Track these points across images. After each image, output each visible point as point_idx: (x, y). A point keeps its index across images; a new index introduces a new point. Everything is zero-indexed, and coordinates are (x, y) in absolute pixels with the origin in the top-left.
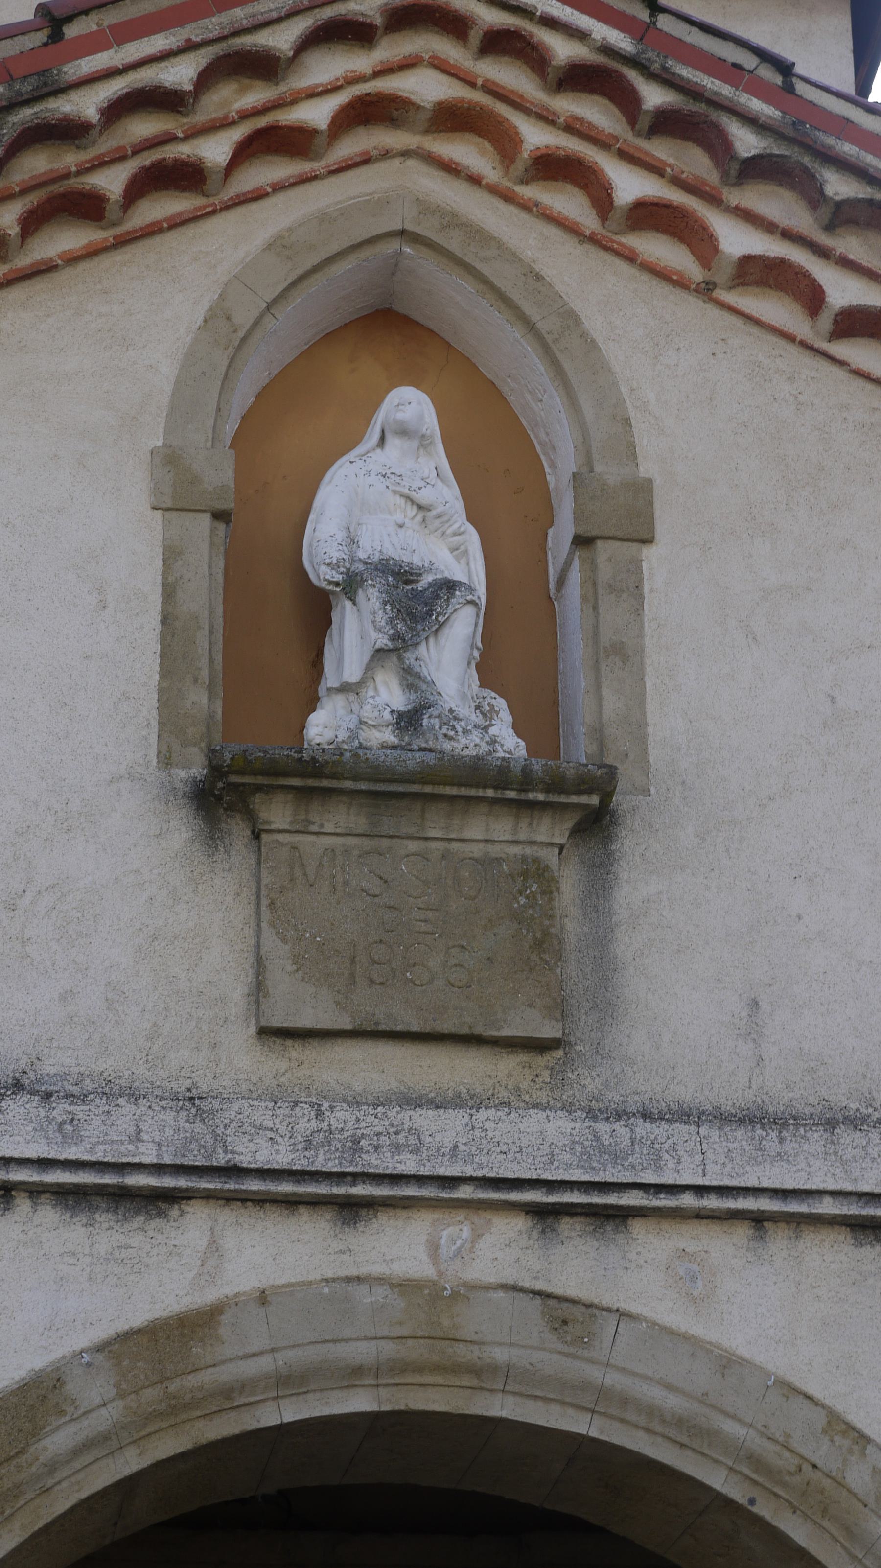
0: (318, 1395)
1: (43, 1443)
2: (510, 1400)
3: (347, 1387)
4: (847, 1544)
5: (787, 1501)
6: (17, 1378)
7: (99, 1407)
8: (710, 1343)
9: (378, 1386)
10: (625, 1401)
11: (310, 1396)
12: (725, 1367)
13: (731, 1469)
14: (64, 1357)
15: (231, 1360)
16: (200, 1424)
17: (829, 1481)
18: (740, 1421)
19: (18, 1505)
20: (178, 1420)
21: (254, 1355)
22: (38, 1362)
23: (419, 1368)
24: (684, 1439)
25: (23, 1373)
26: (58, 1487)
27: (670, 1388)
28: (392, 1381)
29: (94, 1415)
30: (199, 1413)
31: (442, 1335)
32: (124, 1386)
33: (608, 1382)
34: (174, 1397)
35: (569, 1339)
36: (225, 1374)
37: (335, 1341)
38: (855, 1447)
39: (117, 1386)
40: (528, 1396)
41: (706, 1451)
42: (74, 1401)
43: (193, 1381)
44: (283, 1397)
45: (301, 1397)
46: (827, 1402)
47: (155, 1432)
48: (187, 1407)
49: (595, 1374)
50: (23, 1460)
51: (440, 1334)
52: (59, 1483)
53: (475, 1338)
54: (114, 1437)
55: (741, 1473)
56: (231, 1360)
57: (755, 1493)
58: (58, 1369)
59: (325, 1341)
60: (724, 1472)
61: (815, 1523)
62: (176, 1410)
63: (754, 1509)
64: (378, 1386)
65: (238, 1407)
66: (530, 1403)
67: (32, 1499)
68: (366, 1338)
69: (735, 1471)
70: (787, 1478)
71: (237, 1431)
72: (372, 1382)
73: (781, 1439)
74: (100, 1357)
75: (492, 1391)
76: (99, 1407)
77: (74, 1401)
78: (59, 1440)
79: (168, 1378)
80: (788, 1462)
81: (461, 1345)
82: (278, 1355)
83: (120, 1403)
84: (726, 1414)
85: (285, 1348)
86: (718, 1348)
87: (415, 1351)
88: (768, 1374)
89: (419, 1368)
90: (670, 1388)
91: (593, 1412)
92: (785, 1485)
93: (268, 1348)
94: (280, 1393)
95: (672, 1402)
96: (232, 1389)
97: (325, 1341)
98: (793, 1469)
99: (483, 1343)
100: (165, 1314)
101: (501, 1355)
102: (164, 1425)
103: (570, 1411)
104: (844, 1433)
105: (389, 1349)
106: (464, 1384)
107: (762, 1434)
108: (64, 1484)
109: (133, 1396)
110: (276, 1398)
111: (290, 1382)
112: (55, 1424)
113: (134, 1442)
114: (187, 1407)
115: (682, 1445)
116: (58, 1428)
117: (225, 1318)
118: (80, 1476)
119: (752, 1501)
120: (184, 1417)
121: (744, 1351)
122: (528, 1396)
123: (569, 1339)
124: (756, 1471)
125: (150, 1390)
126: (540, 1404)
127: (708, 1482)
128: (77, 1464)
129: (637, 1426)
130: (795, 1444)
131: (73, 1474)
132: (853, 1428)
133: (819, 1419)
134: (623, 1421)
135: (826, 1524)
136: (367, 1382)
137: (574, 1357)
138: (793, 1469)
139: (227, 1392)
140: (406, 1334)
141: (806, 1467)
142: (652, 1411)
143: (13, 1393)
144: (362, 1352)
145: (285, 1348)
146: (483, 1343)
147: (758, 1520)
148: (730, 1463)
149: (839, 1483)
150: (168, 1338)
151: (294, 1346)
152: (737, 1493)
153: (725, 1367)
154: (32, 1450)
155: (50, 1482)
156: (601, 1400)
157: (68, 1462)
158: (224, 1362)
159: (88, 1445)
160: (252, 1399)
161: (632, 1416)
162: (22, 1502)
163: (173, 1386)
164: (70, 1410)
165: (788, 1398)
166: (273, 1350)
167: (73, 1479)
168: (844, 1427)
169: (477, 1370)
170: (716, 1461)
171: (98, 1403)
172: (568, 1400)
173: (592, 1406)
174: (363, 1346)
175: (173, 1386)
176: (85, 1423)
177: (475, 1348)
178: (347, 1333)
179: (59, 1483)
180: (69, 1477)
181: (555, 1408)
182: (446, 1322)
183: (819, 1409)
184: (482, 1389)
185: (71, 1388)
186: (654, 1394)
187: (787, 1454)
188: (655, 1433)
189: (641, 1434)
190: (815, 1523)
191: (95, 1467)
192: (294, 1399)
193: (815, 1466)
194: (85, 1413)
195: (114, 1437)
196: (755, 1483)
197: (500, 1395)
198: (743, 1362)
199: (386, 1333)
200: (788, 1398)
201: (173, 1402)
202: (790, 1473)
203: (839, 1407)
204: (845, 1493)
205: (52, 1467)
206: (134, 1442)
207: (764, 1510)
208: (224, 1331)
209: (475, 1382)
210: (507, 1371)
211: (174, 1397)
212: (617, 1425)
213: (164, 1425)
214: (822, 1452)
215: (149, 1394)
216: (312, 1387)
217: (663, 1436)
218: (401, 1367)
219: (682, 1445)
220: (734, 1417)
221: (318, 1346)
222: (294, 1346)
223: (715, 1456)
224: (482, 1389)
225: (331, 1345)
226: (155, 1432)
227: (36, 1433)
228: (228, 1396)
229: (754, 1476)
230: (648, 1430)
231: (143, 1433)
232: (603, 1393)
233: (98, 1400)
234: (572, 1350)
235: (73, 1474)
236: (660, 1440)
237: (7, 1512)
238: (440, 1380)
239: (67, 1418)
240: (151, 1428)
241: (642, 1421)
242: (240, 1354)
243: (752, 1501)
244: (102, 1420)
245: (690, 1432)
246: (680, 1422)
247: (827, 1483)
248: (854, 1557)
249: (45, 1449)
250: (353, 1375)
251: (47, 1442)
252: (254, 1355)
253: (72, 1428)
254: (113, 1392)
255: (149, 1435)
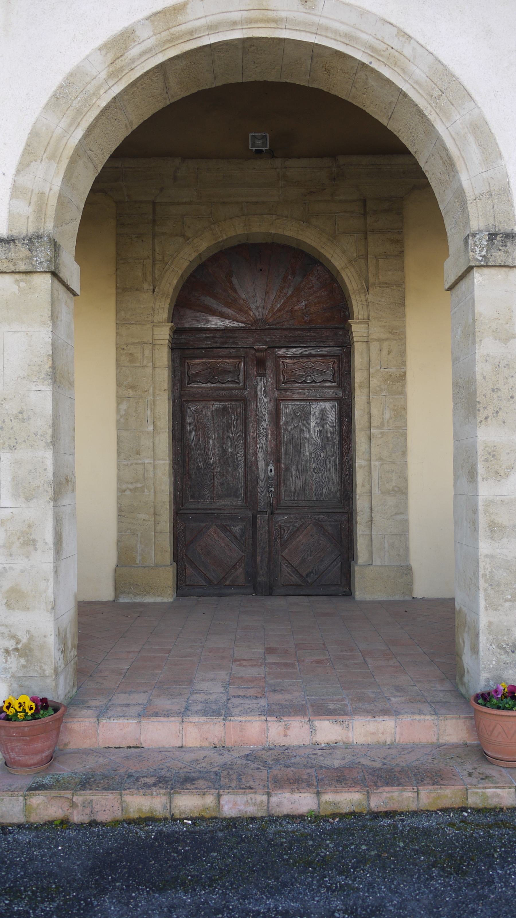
0: (223, 33)
1: (129, 52)
2: (288, 31)
3: (232, 30)
4: (403, 76)
5: (383, 62)
6: (119, 30)
7: (147, 39)
8: (356, 6)
9: (242, 29)
10: (327, 29)
11: (219, 34)
12: (362, 15)
13: (364, 52)
14: (135, 22)
15: (191, 21)
16: (183, 45)
17: (397, 53)
18: (367, 33)
19: (123, 75)
20: (175, 44)
21: (199, 18)
22: (126, 24)
23: (256, 21)
24: (347, 42)
25: (121, 28)
26: (136, 68)
27: (342, 23)
28: (247, 27)
29: (145, 42)
30: (182, 41)
31: (263, 8)
32: (155, 31)
33: (321, 22)
34: (173, 35)
35: (307, 7)
36: (189, 26)
37: (226, 12)
38: (407, 41)
39: (153, 31)
40: (294, 30)
41: (355, 46)
42: (139, 37)
43: (178, 28)
44: (210, 34)
45: (217, 34)
46: (398, 25)
47: (168, 48)
48: (178, 38)
49: (316, 19)
50: (122, 58)
51: (262, 8)
52: (136, 66)
53: (274, 9)
54: (153, 50)
55: (367, 53)
56: (191, 21)
57: (372, 60)
58: (133, 27)
59: (223, 13)
60: (361, 53)
61: (393, 69)
62: (173, 40)
63: (371, 65)
64: (242, 29)
65: (195, 38)
66: (295, 32)
67: (128, 73)
68: (237, 11)
69: (365, 53)
70: (383, 53)
71: (195, 47)
72: (241, 27)
73: (381, 39)
74: (147, 22)
75: (281, 29)
76: (147, 39)
77: (139, 37)
78: (134, 51)
79: (170, 28)
80: (383, 47)
81: (270, 11)
82: (207, 18)
83: (154, 37)
84: (361, 31)
85: (209, 15)
86: (360, 8)
87: (254, 14)
88: (376, 15)
89: (256, 21)
90: (342, 23)
91: (316, 34)
92: (382, 56)
93: (204, 16)
94: (209, 33)
95: (343, 28)
96: (192, 32)
97: (223, 13)
98: (384, 49)
99: (277, 10)
100: (168, 6)
101: (283, 14)
102: (493, 785)
103: (308, 34)
104: (403, 36)
105: (245, 14)
106: (272, 26)
107: (374, 37)
108: (138, 67)
109: (159, 35)
110: (208, 35)
111: (212, 28)
112: (133, 45)
113: (161, 52)
114: (178, 38)
115: (347, 44)
116: (134, 47)
117: (189, 6)
118: (143, 64)
119: (371, 63)
120: (177, 42)
121: (368, 8)
122: (294, 30)
123: (307, 7)
124: (372, 52)
125: (164, 33)
126: (298, 32)
127: (356, 57)
128: (142, 60)
129: (331, 39)
130: (385, 41)
131: (141, 63)
132: (406, 34)
133: (394, 31)
134: (326, 37)
135: (396, 69)
136: (239, 28)
137: (310, 14)
138: (384, 49)
139: (191, 32)
140: (251, 8)
141: (390, 49)
142: (336, 32)
143: (119, 36)
144: (236, 16)
145: (209, 15)
146: (277, 10)
147: (373, 70)
148: (363, 50)
149: (401, 54)
150: (170, 14)
151: (212, 15)
152: (365, 60)
153: (362, 15)
154: (126, 55)
155: (133, 67)
156: (319, 29)
157: (138, 59)
158: (189, 21)
159: (144, 53)
160: (200, 35)
161: (329, 35)
162: (124, 73)
163: (172, 31)
164: (137, 40)
165: (384, 24)
166: (205, 16)
167: (141, 65)
168: (403, 34)
169: (275, 21)
170: (358, 49)
171: (147, 38)
172: (308, 30)
173: (315, 32)
174: (236, 13)
175: (172, 31)
176: (143, 44)
177: (275, 12)
178: (231, 9)
179: (136, 66)
180: (139, 65)
181: (303, 34)
182: (264, 3)
183: (395, 28)
184: (278, 28)
185: (137, 33)
186: (336, 25)
187: (383, 44)
188: (337, 41)
189: (333, 41)
190: (393, 69)
191: (148, 61)
192: (214, 35)
193: (392, 48)
194: (143, 41)
195: (153, 50)
196: (372, 56)
197: (284, 30)
198: (369, 12)
199: (244, 9)
200: (384, 24)
201: (172, 36)
202: (384, 51)
203: (401, 26)
204: (403, 57)
205: (133, 60)
206: (161, 52)
207: (375, 65)
208: (188, 11)
209: (275, 26)
210: (286, 20)
211: (173, 35)
212: (324, 38)
213: (170, 45)
214: (395, 43)
215: (164, 34)
216: (220, 30)
217: (340, 42)
218: (250, 21)
219: (347, 44)
220: (364, 32)
221: (221, 14)
222: (212, 15)
223: (358, 47)
224: (278, 28)
225: (225, 14)
226: (168, 48)
227: (127, 49)
228: (191, 34)
229: (371, 54)
230: (335, 40)
231: (164, 48)
232: (319, 26)
233: (147, 37)
234: (308, 11)
235: (141, 63)
236: (339, 43)
237: (120, 77)
238: (263, 25)
239: (137, 43)
240: (166, 47)
241: (333, 36)
242: (194, 18)
243: (371, 63)
244: (148, 44)
245: (350, 39)
246: (346, 35)
247: (397, 53)
248: (405, 80)
249: (130, 54)
250: (234, 24)
251: (130, 52)
252: (199, 18)
253: (139, 46)
254: (152, 34)
255: (166, 49)
